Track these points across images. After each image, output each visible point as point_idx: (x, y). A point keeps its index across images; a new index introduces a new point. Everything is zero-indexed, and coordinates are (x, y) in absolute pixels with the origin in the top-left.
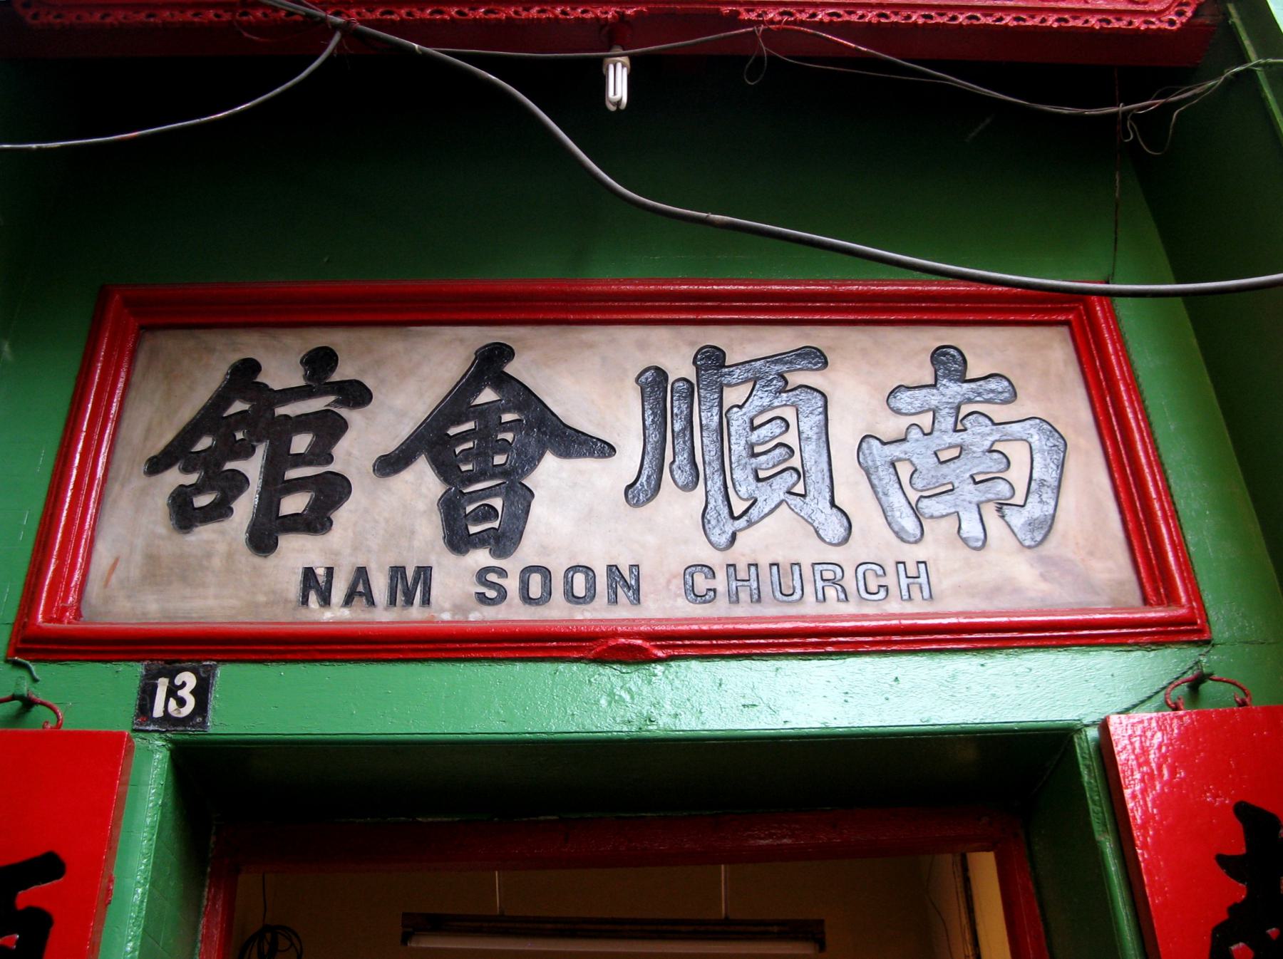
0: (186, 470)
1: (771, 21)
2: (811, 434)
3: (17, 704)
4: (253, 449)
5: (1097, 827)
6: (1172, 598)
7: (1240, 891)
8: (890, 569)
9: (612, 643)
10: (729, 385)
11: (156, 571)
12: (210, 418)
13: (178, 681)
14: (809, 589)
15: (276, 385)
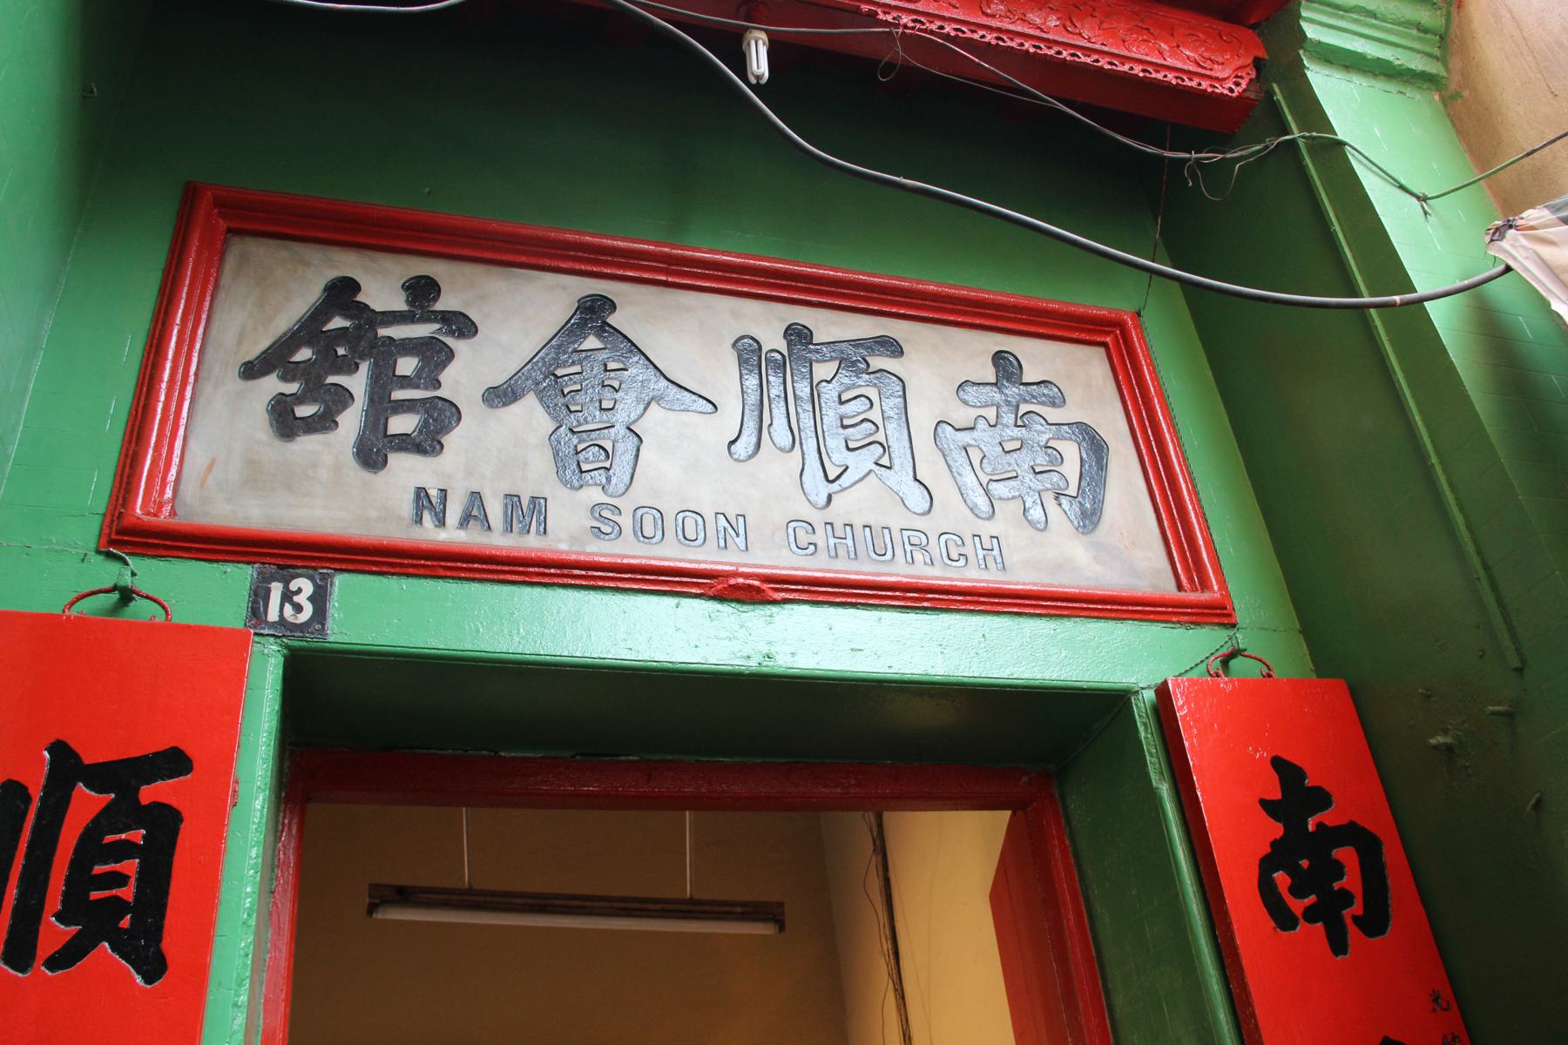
0: (284, 378)
1: (905, 26)
2: (891, 413)
3: (116, 596)
4: (357, 367)
5: (1154, 777)
6: (1205, 585)
7: (1277, 830)
8: (968, 541)
9: (732, 581)
10: (818, 361)
11: (255, 476)
12: (309, 329)
13: (293, 586)
14: (899, 551)
15: (378, 306)
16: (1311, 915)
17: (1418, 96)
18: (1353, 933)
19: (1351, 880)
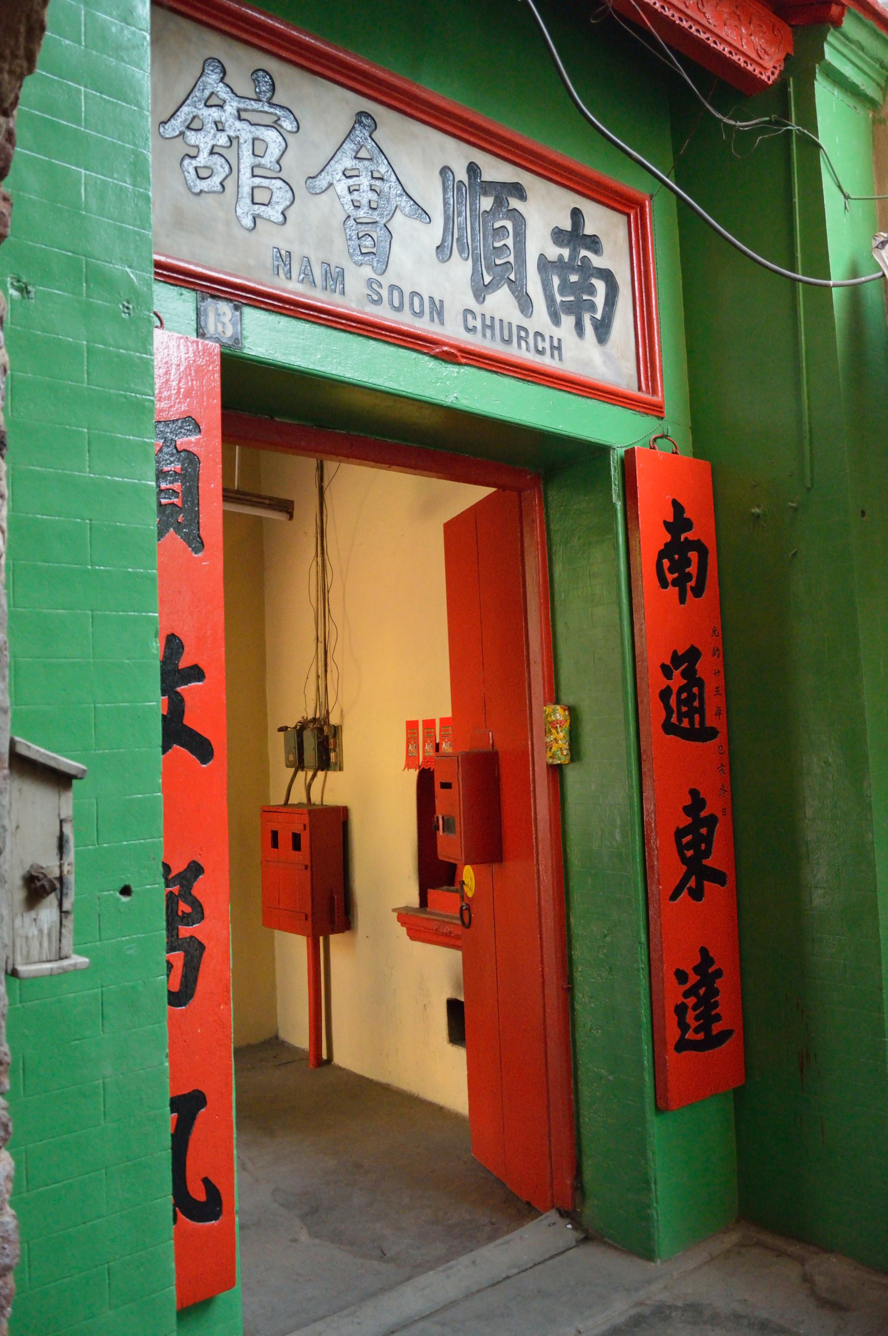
5: (614, 496)
6: (654, 392)
7: (668, 538)
16: (675, 583)
17: (862, 113)
18: (689, 593)
19: (693, 569)
